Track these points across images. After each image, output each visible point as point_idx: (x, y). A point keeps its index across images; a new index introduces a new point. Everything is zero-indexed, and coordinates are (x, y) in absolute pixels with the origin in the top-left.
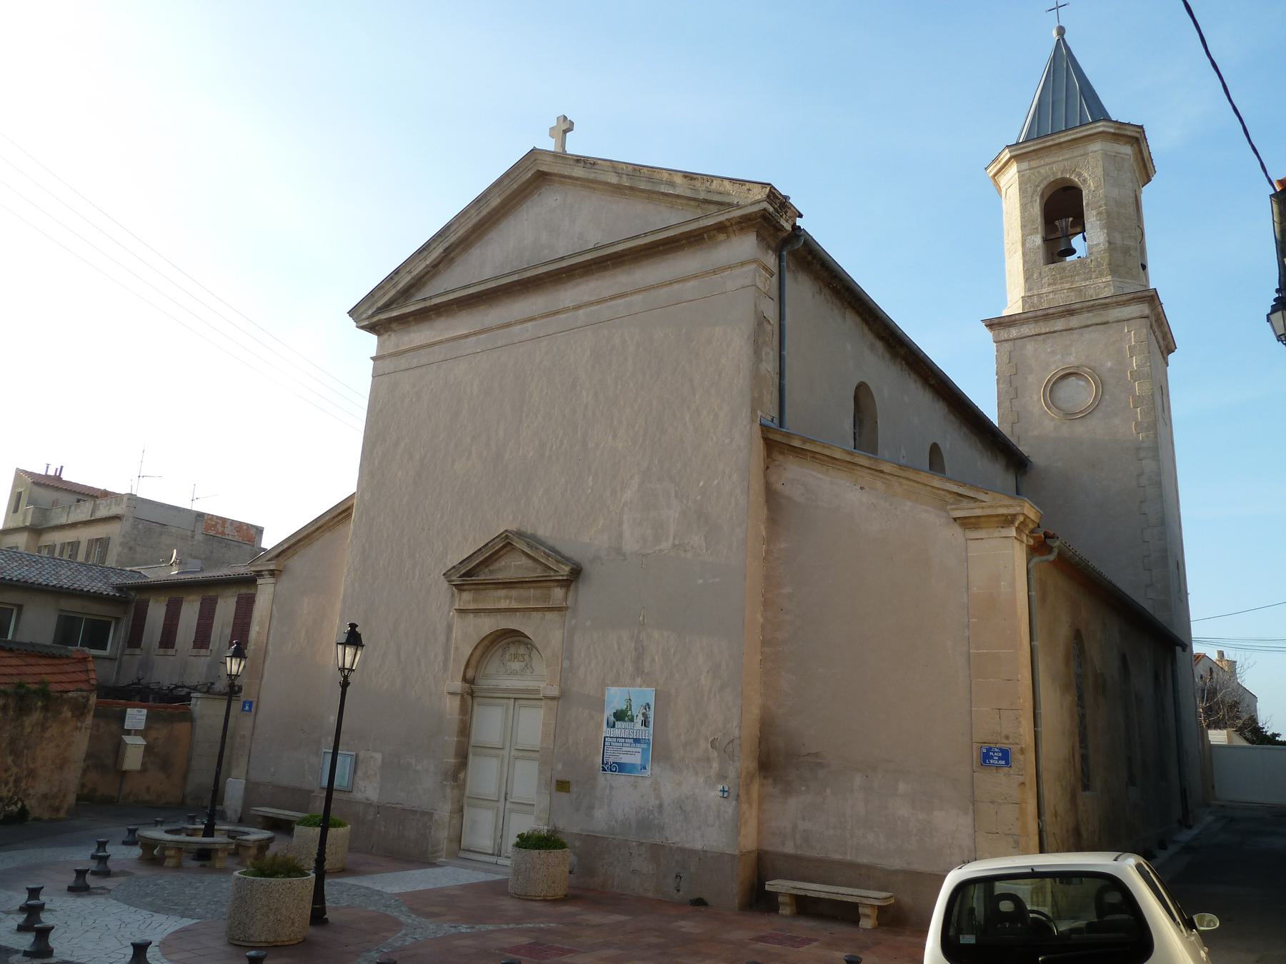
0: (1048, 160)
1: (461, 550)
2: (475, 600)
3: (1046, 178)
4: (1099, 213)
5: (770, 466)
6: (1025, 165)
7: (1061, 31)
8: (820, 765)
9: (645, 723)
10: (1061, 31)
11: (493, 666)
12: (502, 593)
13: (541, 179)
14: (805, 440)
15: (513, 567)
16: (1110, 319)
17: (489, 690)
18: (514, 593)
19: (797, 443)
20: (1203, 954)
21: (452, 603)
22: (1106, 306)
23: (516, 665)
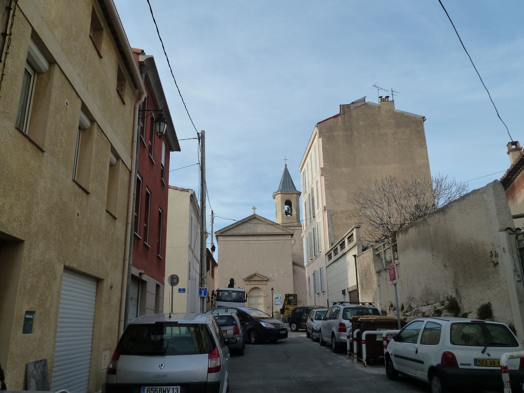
0: (287, 195)
1: (246, 276)
2: (249, 283)
3: (286, 199)
4: (295, 208)
5: (379, 287)
6: (282, 195)
7: (286, 165)
8: (301, 302)
9: (280, 299)
10: (286, 165)
11: (252, 292)
12: (255, 282)
13: (255, 218)
14: (298, 264)
15: (256, 278)
16: (297, 229)
17: (252, 296)
18: (257, 282)
19: (297, 264)
20: (521, 183)
21: (244, 283)
22: (296, 226)
23: (256, 292)
